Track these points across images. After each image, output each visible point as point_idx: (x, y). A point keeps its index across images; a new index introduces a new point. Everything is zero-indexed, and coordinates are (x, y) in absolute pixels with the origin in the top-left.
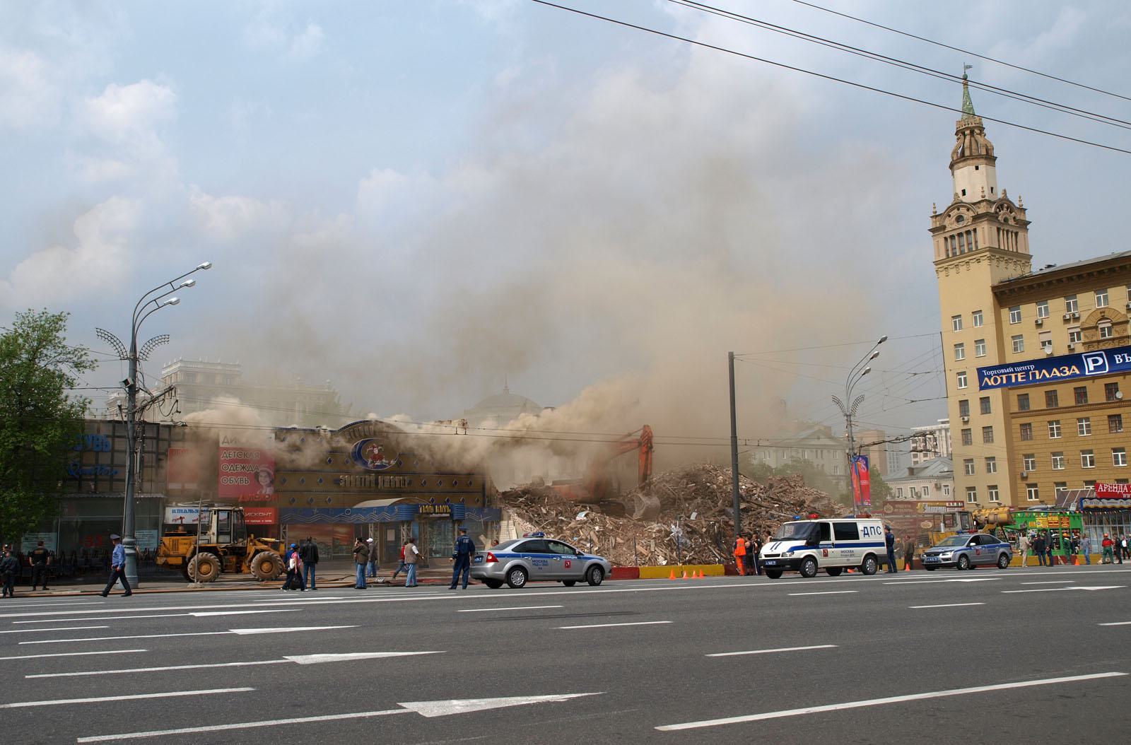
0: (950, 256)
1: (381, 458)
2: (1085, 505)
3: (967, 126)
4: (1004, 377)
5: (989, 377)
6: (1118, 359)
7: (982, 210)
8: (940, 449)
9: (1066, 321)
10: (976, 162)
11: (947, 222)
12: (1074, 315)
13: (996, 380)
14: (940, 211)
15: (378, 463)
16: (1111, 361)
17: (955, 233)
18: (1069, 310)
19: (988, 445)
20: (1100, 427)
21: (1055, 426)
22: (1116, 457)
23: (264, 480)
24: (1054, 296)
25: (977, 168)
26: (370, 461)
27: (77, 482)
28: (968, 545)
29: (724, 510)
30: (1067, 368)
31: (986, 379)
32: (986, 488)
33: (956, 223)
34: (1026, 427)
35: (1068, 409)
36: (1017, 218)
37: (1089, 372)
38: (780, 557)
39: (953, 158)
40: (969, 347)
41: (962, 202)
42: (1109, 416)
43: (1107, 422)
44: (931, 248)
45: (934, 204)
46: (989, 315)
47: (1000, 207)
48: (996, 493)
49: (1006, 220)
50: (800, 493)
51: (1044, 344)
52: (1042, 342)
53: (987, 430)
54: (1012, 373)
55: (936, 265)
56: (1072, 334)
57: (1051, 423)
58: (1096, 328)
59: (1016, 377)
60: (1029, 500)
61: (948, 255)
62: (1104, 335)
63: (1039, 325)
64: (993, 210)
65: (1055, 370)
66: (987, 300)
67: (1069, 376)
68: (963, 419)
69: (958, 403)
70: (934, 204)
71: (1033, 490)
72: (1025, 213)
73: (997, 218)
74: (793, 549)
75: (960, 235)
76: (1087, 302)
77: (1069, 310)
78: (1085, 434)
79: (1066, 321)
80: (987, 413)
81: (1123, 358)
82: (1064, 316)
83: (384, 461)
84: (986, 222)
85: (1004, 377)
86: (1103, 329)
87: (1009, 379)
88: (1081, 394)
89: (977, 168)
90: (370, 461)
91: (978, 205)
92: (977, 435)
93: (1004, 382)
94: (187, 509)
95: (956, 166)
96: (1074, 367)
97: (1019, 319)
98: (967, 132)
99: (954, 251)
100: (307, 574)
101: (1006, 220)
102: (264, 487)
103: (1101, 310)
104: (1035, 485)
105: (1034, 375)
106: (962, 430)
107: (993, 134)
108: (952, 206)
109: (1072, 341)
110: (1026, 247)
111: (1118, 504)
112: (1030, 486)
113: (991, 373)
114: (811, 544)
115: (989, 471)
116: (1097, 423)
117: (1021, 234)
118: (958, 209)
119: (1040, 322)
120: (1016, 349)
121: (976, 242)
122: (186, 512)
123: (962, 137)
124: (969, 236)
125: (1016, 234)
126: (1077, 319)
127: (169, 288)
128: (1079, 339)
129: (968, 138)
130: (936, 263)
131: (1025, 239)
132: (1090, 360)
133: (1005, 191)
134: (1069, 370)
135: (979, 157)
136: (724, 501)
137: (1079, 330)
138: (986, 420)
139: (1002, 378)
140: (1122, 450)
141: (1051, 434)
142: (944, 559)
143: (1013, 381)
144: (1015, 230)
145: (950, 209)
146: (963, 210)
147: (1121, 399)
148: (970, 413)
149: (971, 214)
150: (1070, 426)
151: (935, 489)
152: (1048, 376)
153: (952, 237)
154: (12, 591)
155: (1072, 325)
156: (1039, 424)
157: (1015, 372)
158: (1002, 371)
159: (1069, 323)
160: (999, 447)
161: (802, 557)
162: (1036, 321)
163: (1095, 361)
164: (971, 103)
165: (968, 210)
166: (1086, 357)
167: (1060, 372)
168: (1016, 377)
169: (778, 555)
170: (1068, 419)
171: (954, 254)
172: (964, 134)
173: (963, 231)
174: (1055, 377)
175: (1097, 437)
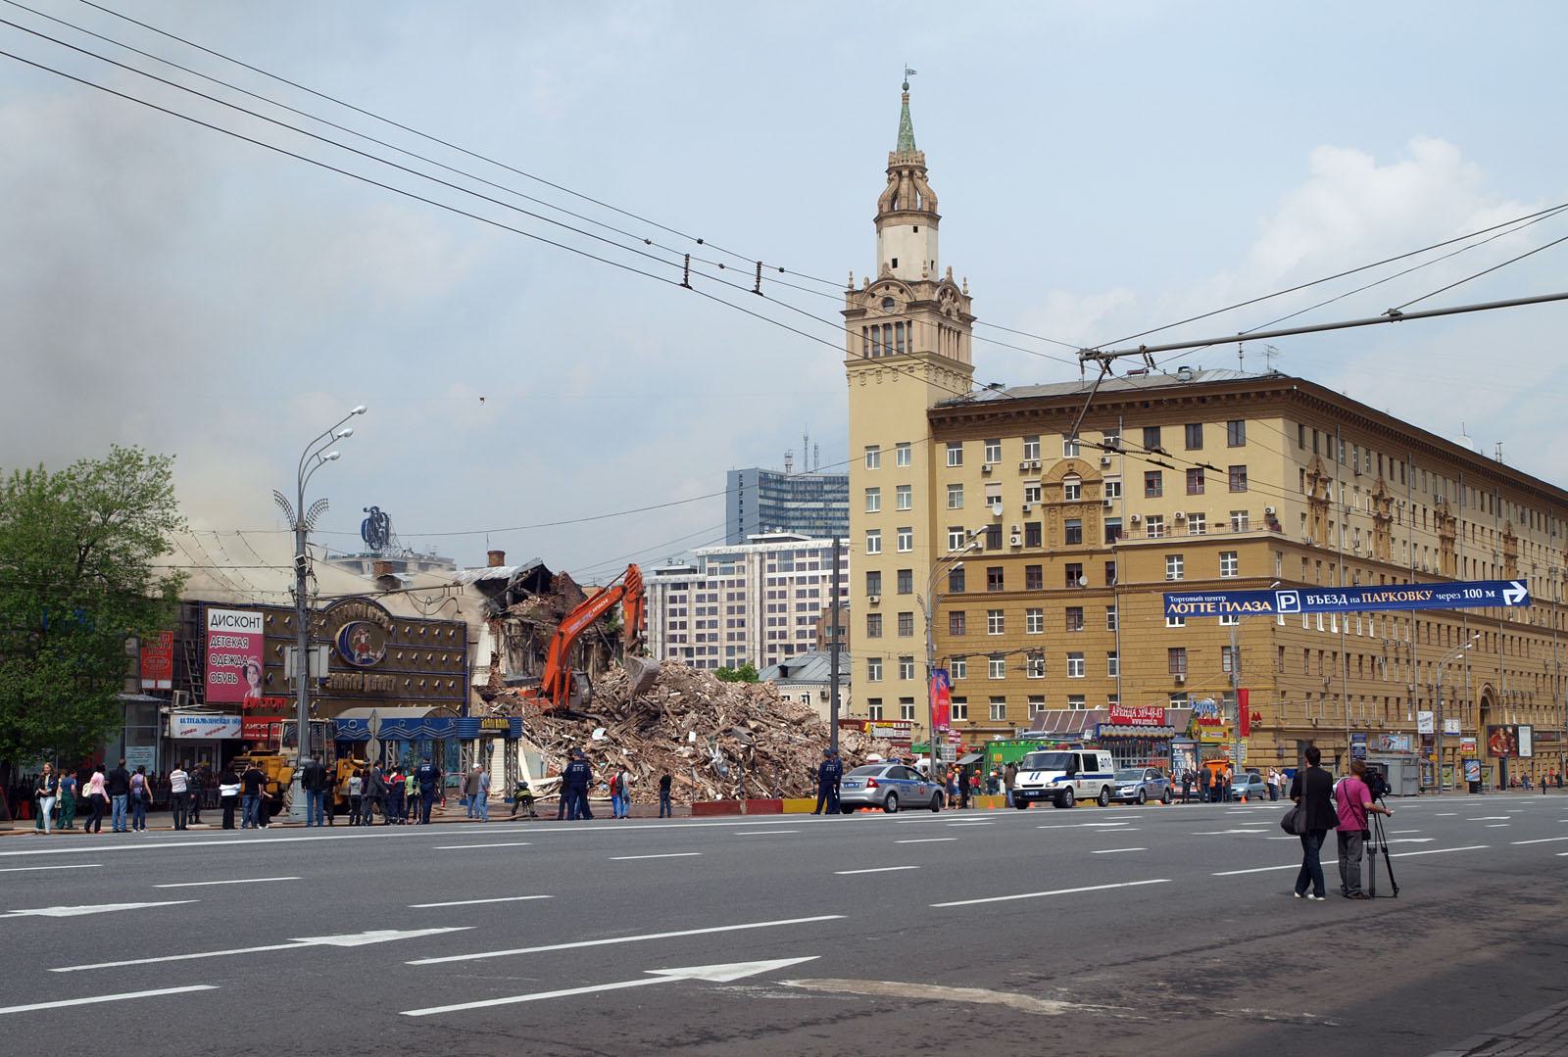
0: (870, 356)
1: (367, 650)
2: (1101, 732)
3: (905, 163)
4: (1192, 605)
5: (1176, 604)
6: (1310, 600)
7: (922, 295)
8: (651, 618)
9: (1024, 471)
10: (915, 220)
11: (869, 303)
12: (1034, 464)
13: (1183, 608)
14: (859, 286)
15: (364, 657)
16: (1304, 601)
17: (880, 323)
18: (1028, 456)
19: (906, 639)
20: (1055, 623)
21: (996, 618)
22: (1072, 664)
23: (252, 678)
24: (1010, 433)
25: (916, 230)
26: (357, 653)
27: (1530, 755)
28: (1145, 780)
29: (730, 730)
30: (1259, 604)
31: (1173, 606)
32: (898, 701)
33: (881, 308)
34: (957, 616)
35: (1016, 596)
36: (962, 311)
37: (1281, 609)
38: (1044, 788)
39: (881, 207)
40: (888, 494)
41: (893, 279)
42: (1068, 609)
43: (1064, 617)
44: (838, 341)
45: (851, 274)
46: (920, 451)
47: (944, 293)
48: (912, 709)
49: (949, 312)
50: (788, 708)
51: (990, 500)
52: (988, 498)
53: (905, 617)
54: (1200, 602)
55: (848, 366)
56: (1029, 491)
57: (991, 613)
58: (1061, 485)
59: (1205, 607)
60: (953, 720)
61: (866, 354)
62: (1069, 496)
63: (986, 473)
64: (935, 297)
65: (1246, 604)
66: (922, 427)
67: (1260, 612)
68: (872, 599)
69: (865, 574)
70: (851, 274)
71: (960, 705)
72: (969, 304)
73: (939, 308)
74: (1056, 780)
75: (887, 326)
76: (1052, 447)
77: (1028, 456)
78: (1035, 632)
79: (1024, 471)
80: (906, 593)
81: (1315, 599)
82: (1022, 465)
83: (371, 653)
84: (927, 314)
85: (1192, 605)
86: (1069, 488)
87: (1197, 608)
88: (1034, 575)
89: (916, 230)
90: (357, 653)
91: (917, 287)
92: (890, 623)
93: (1192, 611)
94: (200, 717)
95: (885, 221)
96: (1266, 603)
97: (960, 461)
98: (905, 173)
99: (876, 349)
100: (409, 808)
101: (949, 312)
102: (253, 687)
103: (1069, 462)
104: (963, 699)
105: (1225, 606)
106: (868, 615)
107: (937, 181)
108: (878, 281)
109: (1028, 500)
110: (969, 356)
111: (1130, 731)
112: (956, 700)
113: (1179, 600)
114: (1070, 776)
115: (903, 676)
116: (1051, 617)
117: (963, 337)
118: (887, 288)
119: (988, 469)
120: (951, 504)
121: (910, 341)
122: (198, 721)
123: (897, 178)
124: (888, 332)
125: (959, 333)
126: (1037, 470)
127: (328, 438)
128: (1038, 497)
129: (905, 182)
130: (848, 363)
131: (968, 343)
132: (1283, 598)
133: (950, 269)
134: (1261, 606)
135: (919, 213)
136: (727, 717)
137: (1038, 485)
138: (907, 603)
139: (1189, 606)
140: (1080, 655)
141: (990, 628)
142: (1126, 794)
143: (1202, 610)
144: (958, 329)
145: (878, 284)
146: (894, 291)
147: (1084, 586)
148: (883, 591)
149: (905, 298)
150: (1017, 619)
151: (820, 700)
152: (1239, 609)
153: (875, 328)
154: (197, 817)
155: (1030, 477)
156: (976, 613)
157: (1204, 601)
158: (1191, 599)
159: (1027, 474)
160: (917, 644)
161: (1064, 787)
162: (984, 467)
163: (1288, 600)
164: (911, 128)
165: (901, 291)
166: (1280, 595)
167: (1252, 607)
168: (1205, 607)
169: (1042, 786)
170: (1014, 610)
171: (876, 354)
172: (900, 174)
173: (892, 321)
174: (1246, 612)
175: (1050, 636)
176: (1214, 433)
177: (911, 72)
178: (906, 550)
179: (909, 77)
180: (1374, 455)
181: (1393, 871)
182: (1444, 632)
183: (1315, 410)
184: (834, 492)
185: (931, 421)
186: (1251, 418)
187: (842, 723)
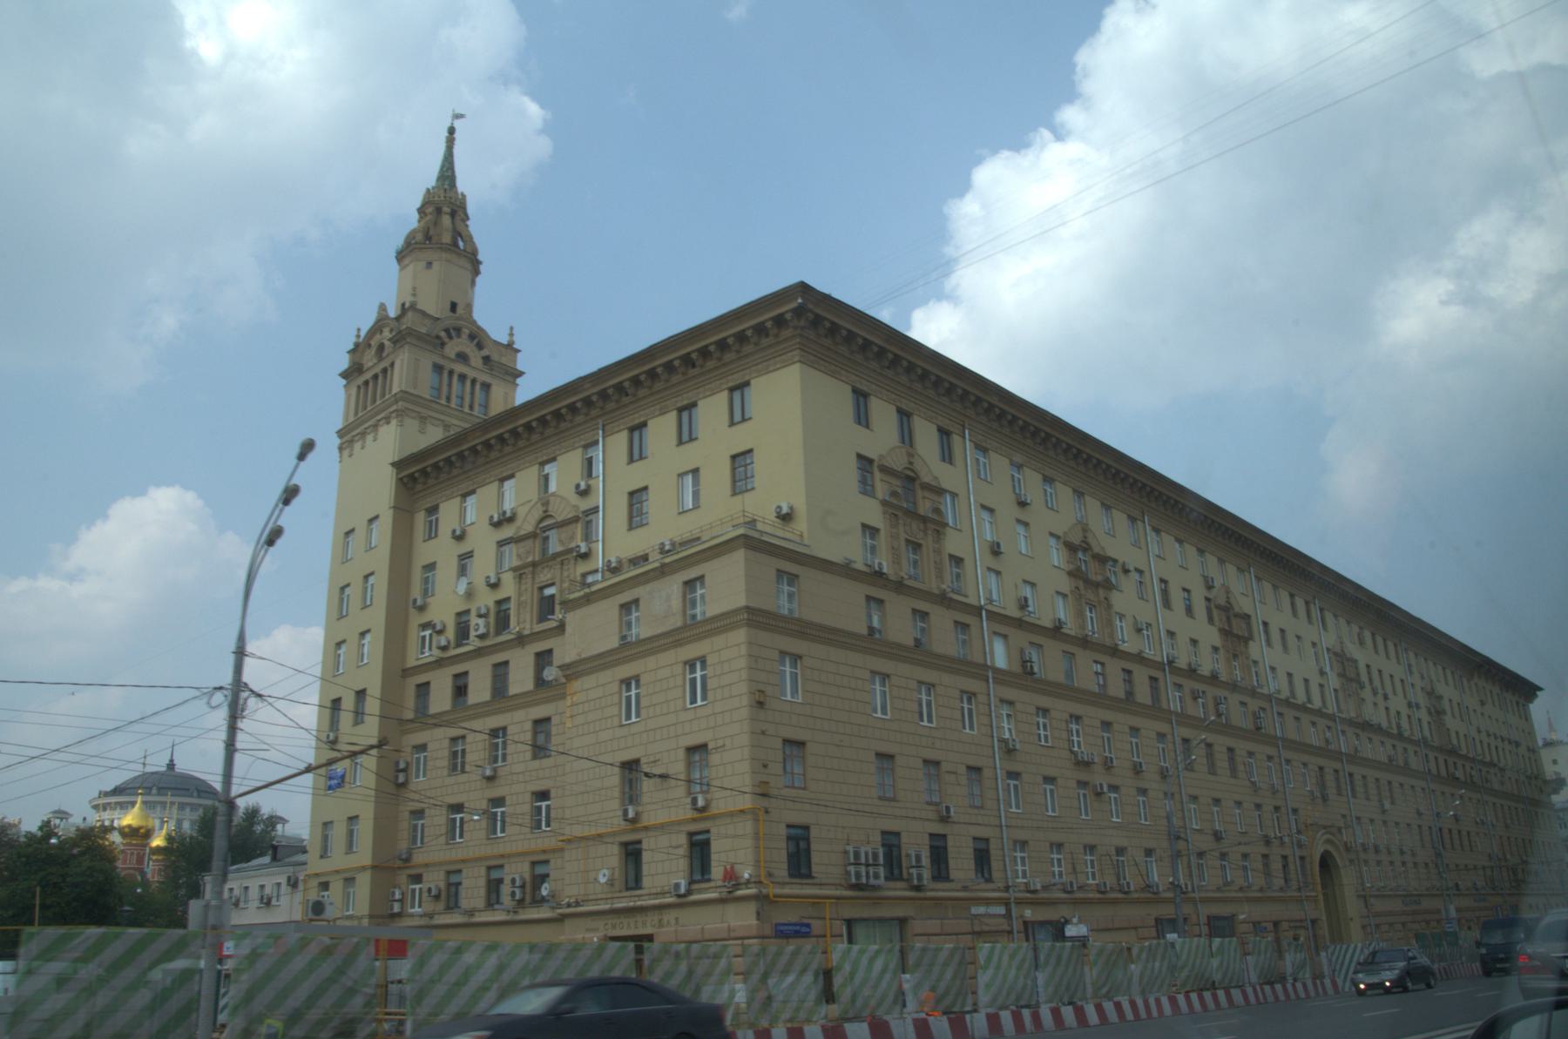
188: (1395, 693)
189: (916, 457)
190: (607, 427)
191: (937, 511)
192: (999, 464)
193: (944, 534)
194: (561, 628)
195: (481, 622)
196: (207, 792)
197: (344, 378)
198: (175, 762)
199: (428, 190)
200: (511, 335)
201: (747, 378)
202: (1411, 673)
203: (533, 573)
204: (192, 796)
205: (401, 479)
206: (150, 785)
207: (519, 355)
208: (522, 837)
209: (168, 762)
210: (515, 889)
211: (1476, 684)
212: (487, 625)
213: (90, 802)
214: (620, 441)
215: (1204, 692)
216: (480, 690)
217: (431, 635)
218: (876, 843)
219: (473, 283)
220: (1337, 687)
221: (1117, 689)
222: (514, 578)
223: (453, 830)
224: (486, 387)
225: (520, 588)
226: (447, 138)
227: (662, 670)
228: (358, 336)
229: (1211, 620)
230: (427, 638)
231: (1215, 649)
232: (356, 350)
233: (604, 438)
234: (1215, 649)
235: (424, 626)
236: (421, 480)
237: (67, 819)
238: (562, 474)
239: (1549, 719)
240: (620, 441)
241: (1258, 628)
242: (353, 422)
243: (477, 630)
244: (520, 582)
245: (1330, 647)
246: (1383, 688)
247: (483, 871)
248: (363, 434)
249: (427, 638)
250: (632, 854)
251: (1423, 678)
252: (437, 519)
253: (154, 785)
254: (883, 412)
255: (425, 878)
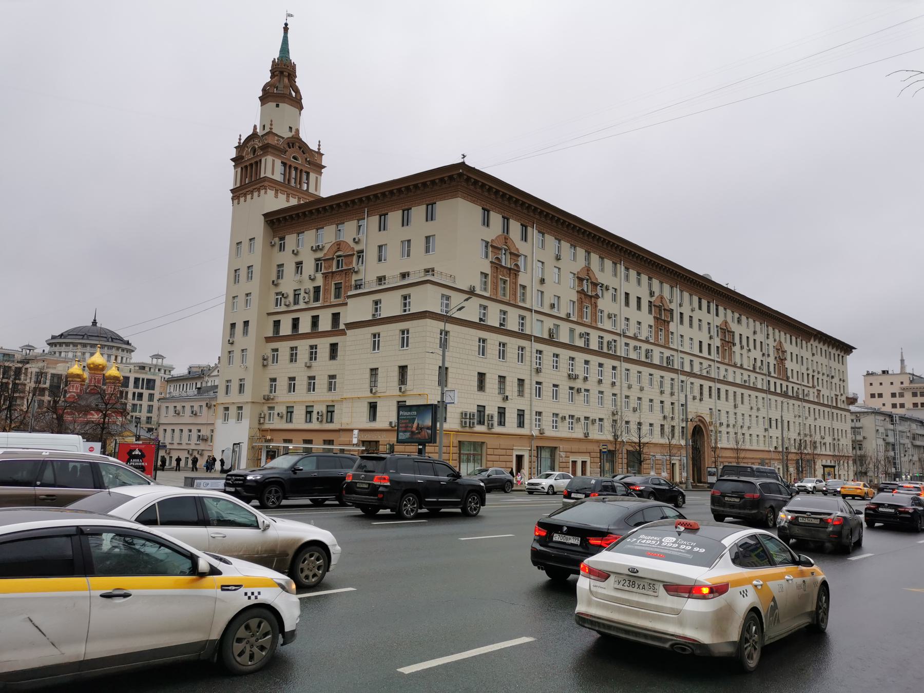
46: (259, 244)
176: (418, 213)
177: (290, 15)
178: (405, 348)
179: (288, 18)
180: (788, 336)
181: (22, 542)
182: (839, 417)
183: (774, 321)
184: (621, 374)
185: (266, 222)
186: (441, 200)
187: (685, 483)
188: (755, 348)
189: (509, 239)
190: (369, 212)
191: (517, 265)
192: (550, 240)
193: (518, 275)
194: (346, 304)
195: (306, 295)
196: (117, 339)
197: (233, 161)
198: (97, 321)
199: (274, 61)
200: (319, 145)
201: (435, 201)
202: (768, 338)
203: (332, 276)
204: (108, 341)
205: (266, 221)
206: (83, 334)
207: (323, 156)
208: (323, 394)
209: (93, 321)
210: (319, 417)
211: (812, 345)
212: (309, 298)
213: (46, 341)
214: (375, 219)
215: (640, 347)
216: (305, 326)
217: (281, 298)
218: (474, 410)
219: (300, 114)
220: (719, 345)
221: (594, 345)
222: (323, 277)
223: (292, 388)
224: (308, 174)
225: (325, 282)
226: (284, 28)
227: (390, 333)
228: (239, 143)
229: (650, 312)
230: (279, 299)
231: (650, 326)
232: (240, 148)
233: (367, 217)
234: (650, 326)
235: (277, 294)
236: (277, 223)
237: (33, 350)
238: (349, 230)
239: (902, 353)
240: (375, 219)
241: (676, 316)
242: (239, 187)
243: (304, 300)
244: (325, 280)
245: (719, 325)
246: (748, 346)
247: (304, 408)
248: (245, 195)
249: (279, 299)
250: (373, 407)
251: (775, 341)
252: (284, 243)
253: (86, 334)
254: (496, 218)
255: (275, 408)
